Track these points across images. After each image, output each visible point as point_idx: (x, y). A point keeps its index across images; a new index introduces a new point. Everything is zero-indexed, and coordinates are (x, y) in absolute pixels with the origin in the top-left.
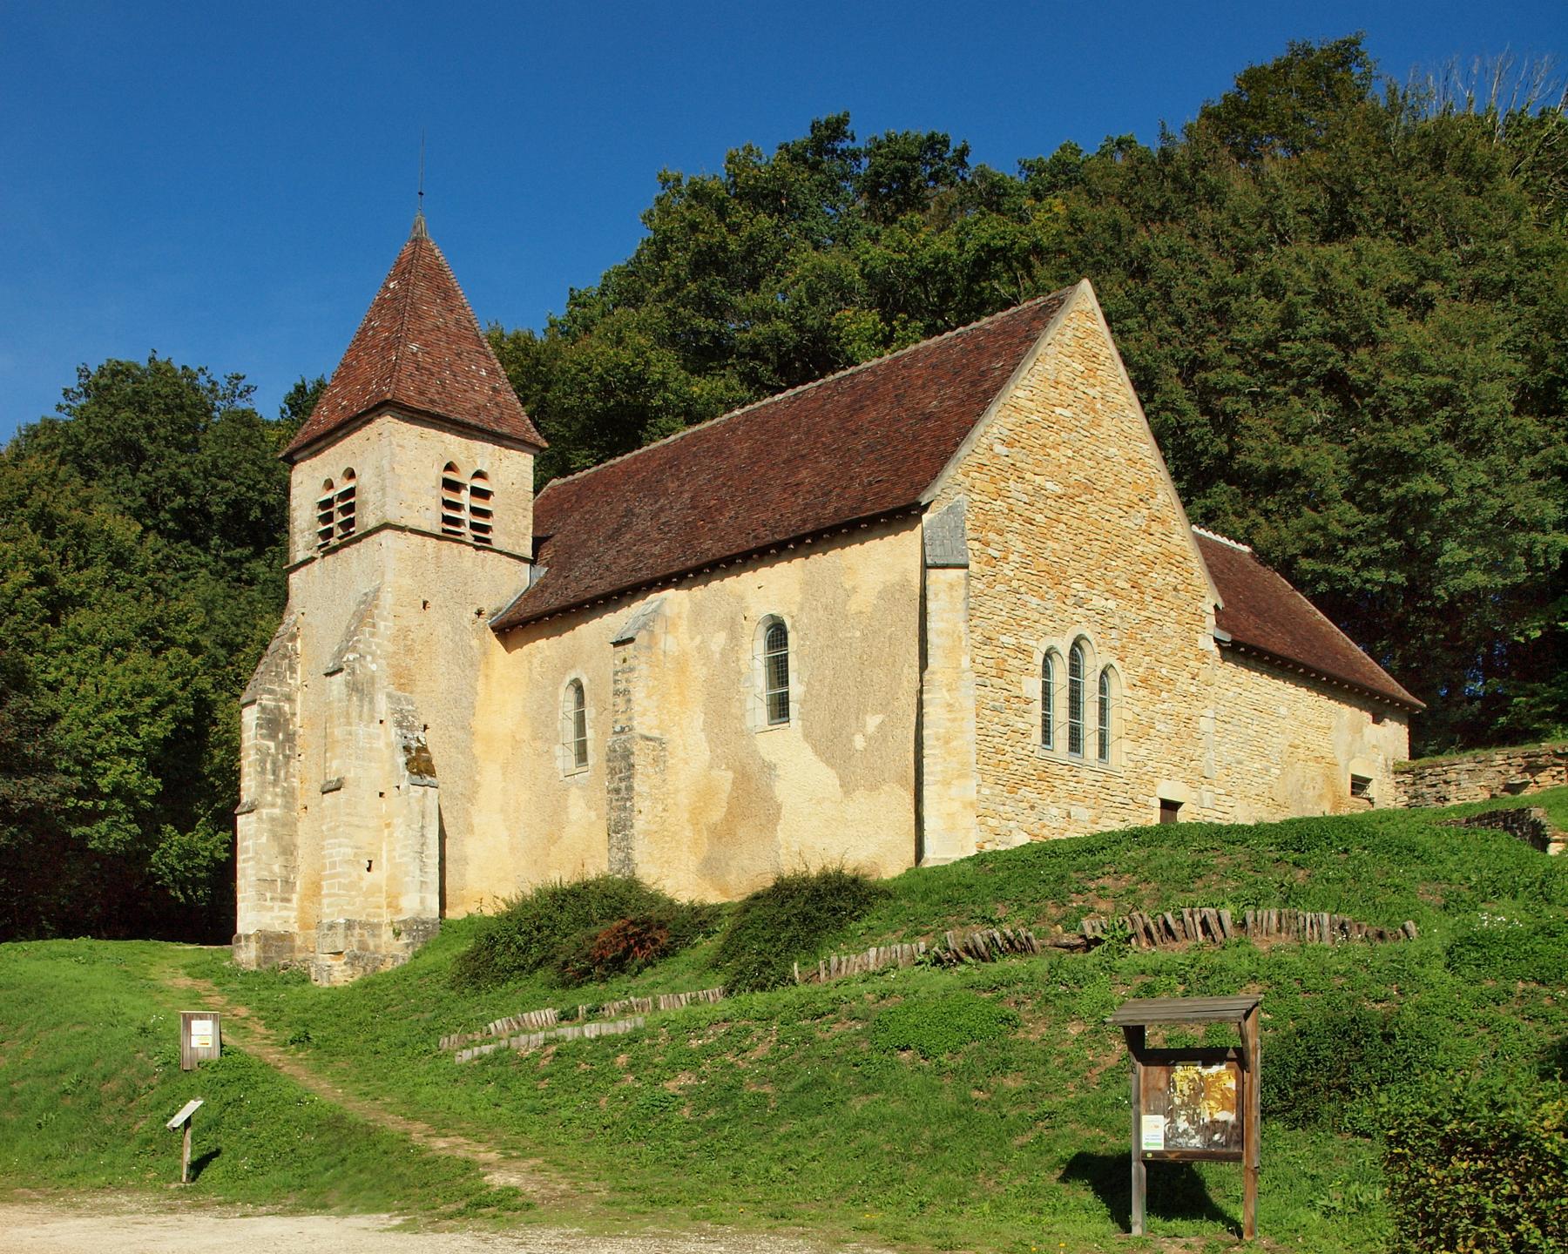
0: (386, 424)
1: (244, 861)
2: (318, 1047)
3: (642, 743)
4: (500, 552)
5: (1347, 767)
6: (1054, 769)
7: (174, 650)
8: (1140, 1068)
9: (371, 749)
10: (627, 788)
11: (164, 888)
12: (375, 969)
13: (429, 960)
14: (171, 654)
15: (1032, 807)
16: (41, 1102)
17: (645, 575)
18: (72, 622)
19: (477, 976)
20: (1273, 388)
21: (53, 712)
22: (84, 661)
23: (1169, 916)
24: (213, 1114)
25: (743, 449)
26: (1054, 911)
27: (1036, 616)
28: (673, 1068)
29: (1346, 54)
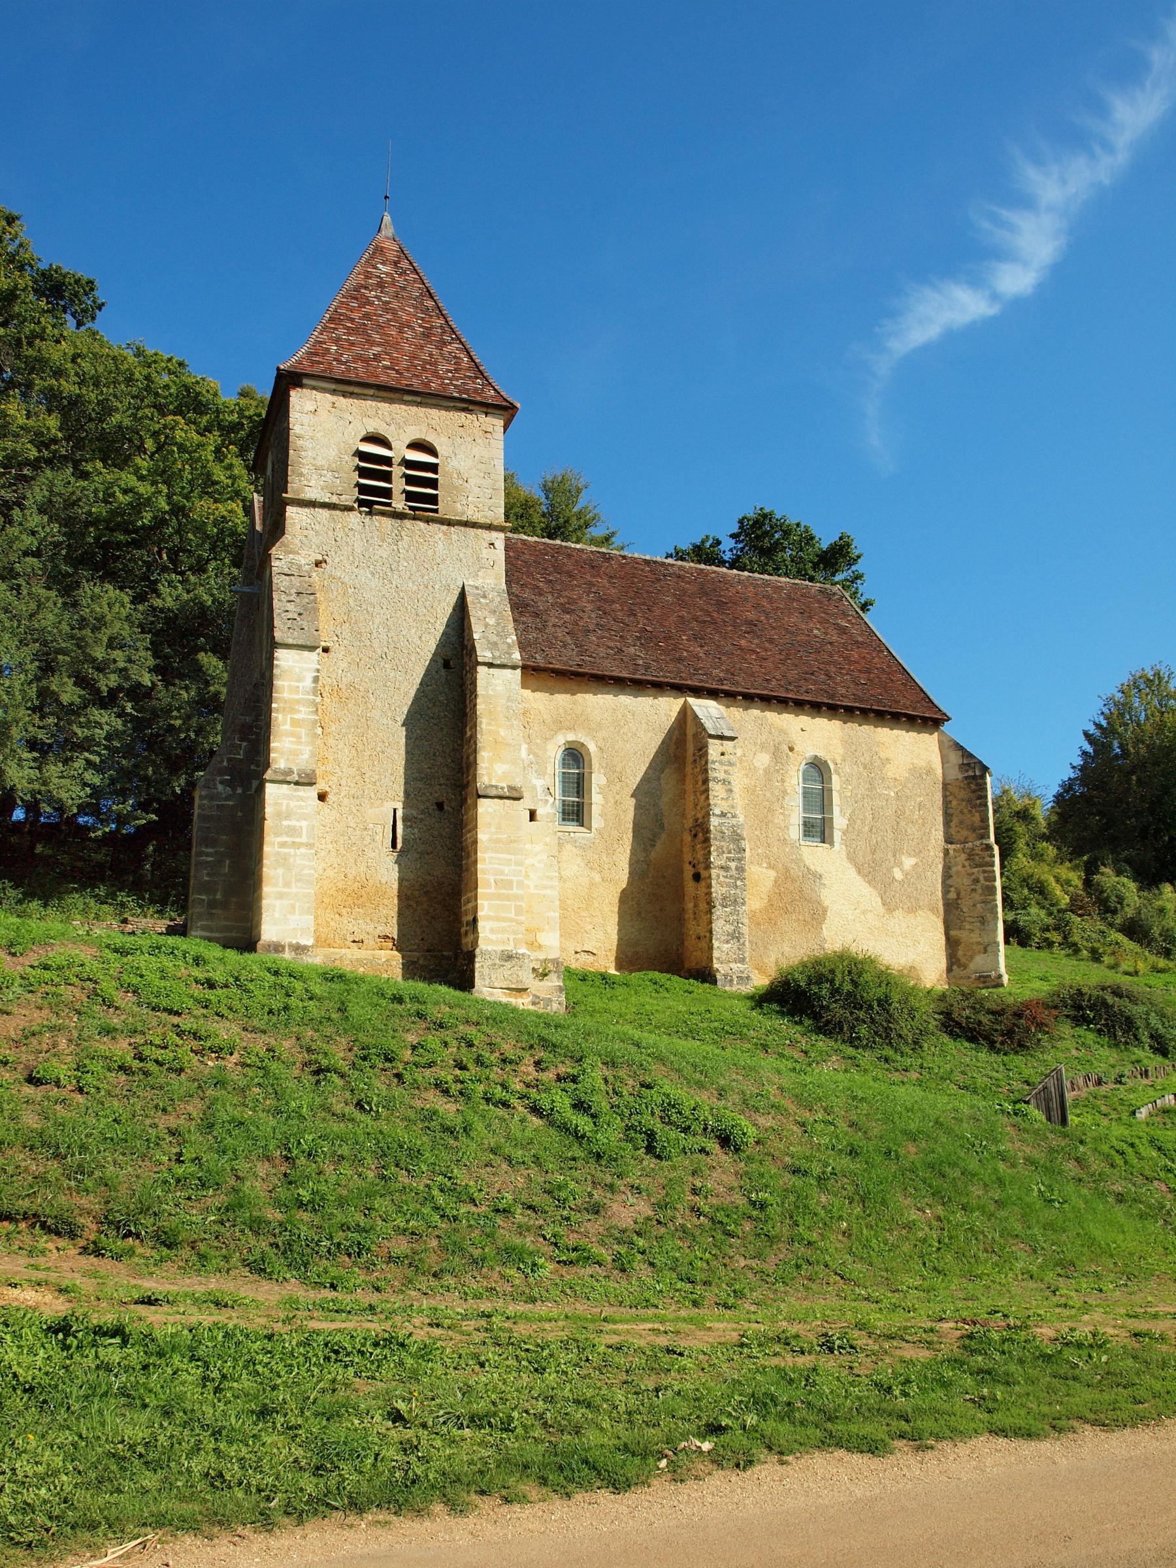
10: (737, 868)
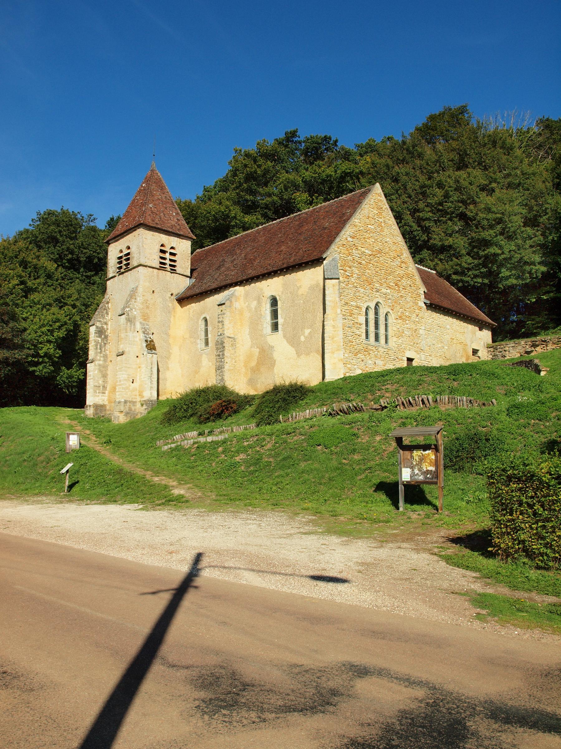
0: (141, 231)
1: (90, 379)
2: (114, 445)
3: (228, 339)
4: (179, 274)
5: (471, 346)
6: (370, 347)
7: (67, 307)
8: (401, 452)
9: (134, 341)
11: (61, 389)
12: (134, 417)
13: (153, 414)
14: (66, 308)
15: (362, 361)
16: (16, 464)
17: (229, 282)
18: (32, 297)
19: (170, 420)
20: (442, 218)
21: (25, 328)
22: (36, 311)
23: (410, 398)
24: (77, 468)
25: (262, 239)
26: (370, 397)
27: (363, 295)
28: (238, 452)
29: (463, 110)
